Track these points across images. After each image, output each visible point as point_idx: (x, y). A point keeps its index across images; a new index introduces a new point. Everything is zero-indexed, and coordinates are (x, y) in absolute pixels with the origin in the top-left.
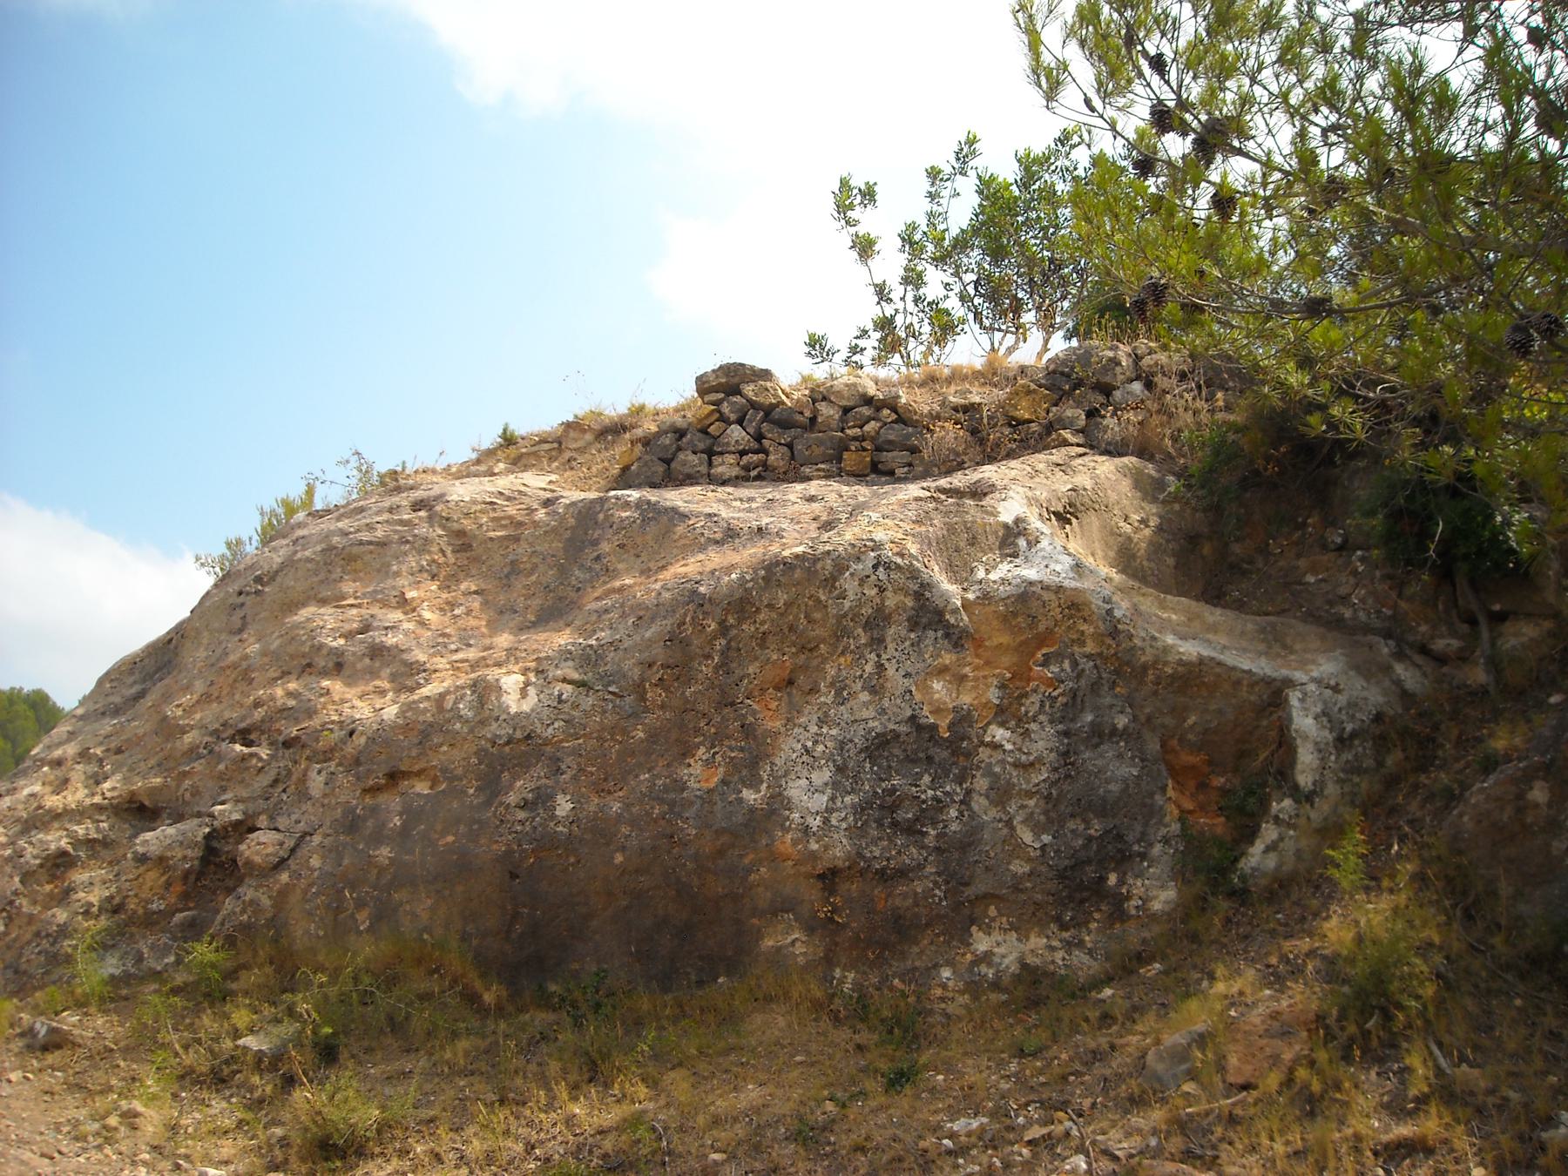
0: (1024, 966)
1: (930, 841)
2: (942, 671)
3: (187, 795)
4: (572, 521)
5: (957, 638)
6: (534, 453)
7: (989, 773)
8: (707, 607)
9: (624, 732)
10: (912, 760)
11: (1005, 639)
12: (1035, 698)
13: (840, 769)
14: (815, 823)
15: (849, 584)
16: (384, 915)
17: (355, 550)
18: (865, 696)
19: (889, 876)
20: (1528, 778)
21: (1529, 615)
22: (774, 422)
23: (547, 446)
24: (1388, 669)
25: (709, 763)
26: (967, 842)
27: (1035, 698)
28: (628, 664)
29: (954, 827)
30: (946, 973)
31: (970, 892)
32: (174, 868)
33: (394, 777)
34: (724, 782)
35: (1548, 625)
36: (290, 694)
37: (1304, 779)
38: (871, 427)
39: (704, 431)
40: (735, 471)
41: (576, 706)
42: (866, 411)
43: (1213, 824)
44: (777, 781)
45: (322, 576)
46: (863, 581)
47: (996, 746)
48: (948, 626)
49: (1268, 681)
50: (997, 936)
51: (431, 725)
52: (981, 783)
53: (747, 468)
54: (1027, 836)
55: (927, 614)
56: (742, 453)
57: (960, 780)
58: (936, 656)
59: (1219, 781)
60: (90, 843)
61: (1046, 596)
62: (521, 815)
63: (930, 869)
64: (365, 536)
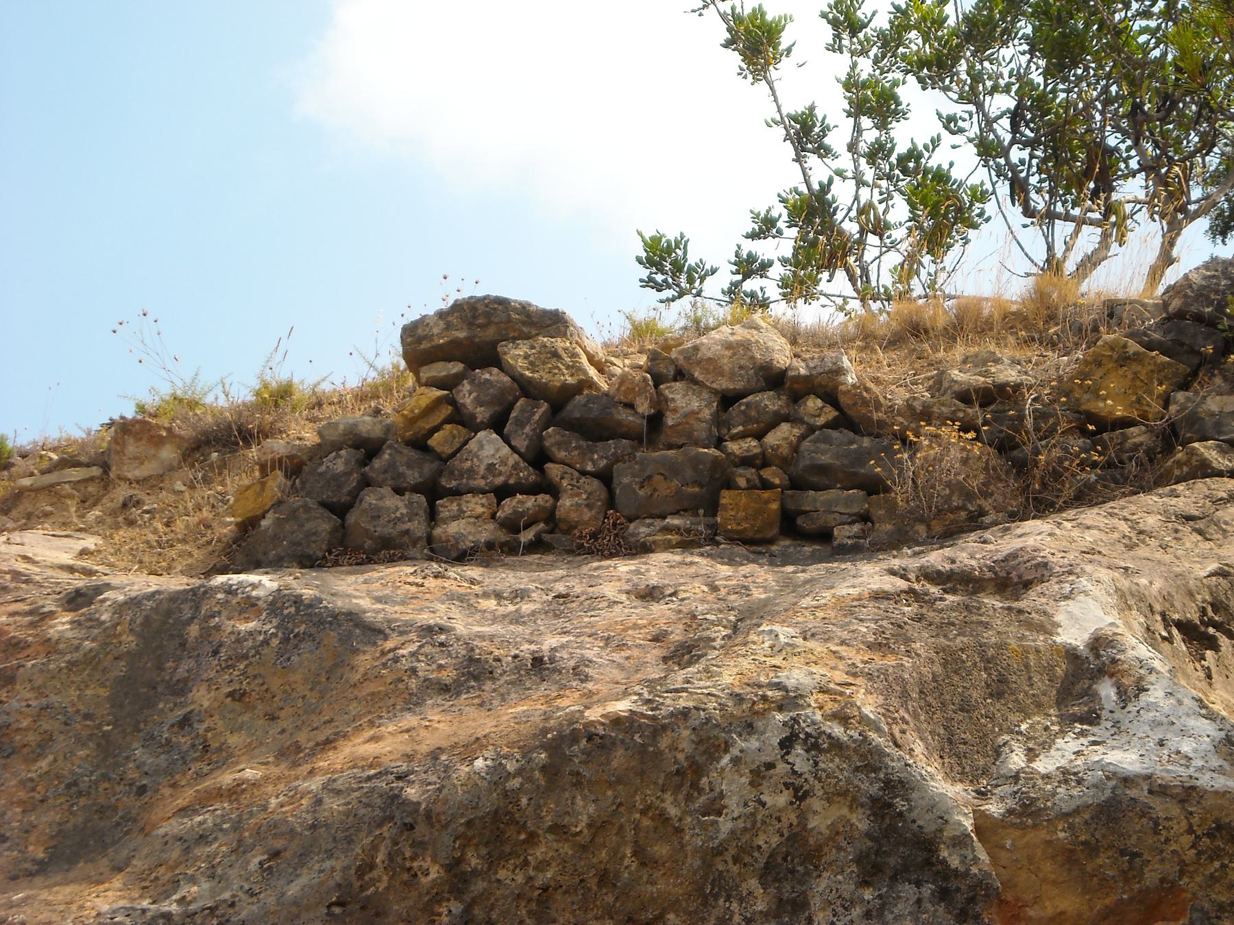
6: (49, 489)
8: (421, 830)
15: (730, 784)
23: (76, 474)
39: (420, 444)
40: (487, 532)
42: (770, 402)
46: (759, 774)
48: (946, 873)
56: (503, 492)
61: (1161, 807)
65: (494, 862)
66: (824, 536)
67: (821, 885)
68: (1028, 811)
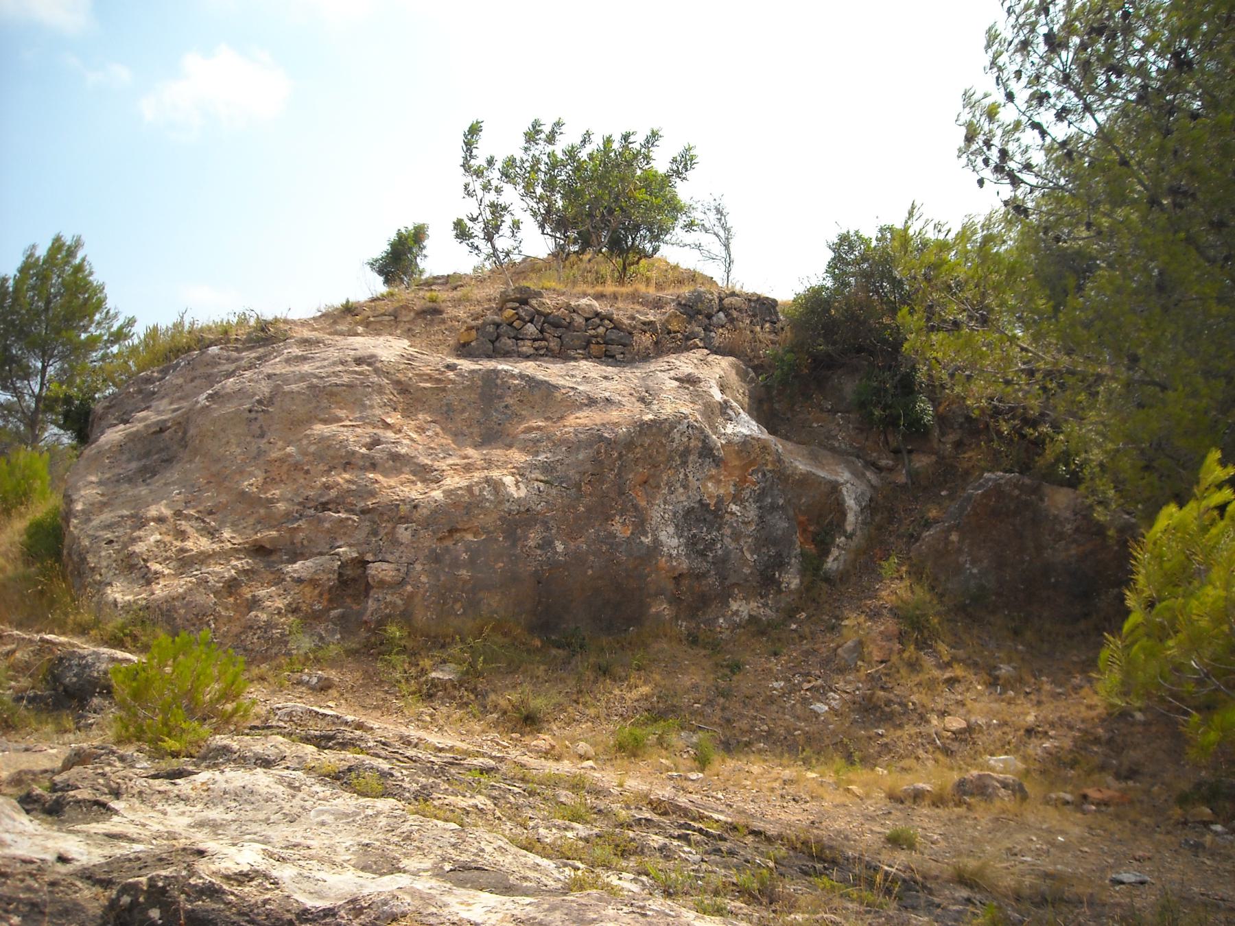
0: (750, 616)
1: (710, 559)
2: (711, 477)
3: (305, 542)
4: (480, 383)
5: (718, 462)
6: (380, 322)
7: (731, 526)
8: (613, 445)
9: (574, 507)
10: (698, 520)
11: (737, 463)
12: (748, 491)
13: (677, 526)
14: (674, 553)
15: (675, 434)
16: (473, 605)
17: (335, 389)
18: (681, 490)
19: (700, 576)
20: (949, 530)
21: (924, 452)
22: (549, 323)
23: (387, 318)
24: (864, 474)
25: (624, 524)
26: (724, 560)
27: (748, 491)
28: (571, 473)
29: (720, 552)
30: (721, 621)
31: (727, 583)
32: (323, 585)
33: (452, 531)
34: (632, 534)
35: (934, 458)
36: (348, 481)
37: (849, 528)
38: (601, 330)
39: (510, 325)
40: (532, 351)
41: (548, 494)
42: (597, 320)
43: (811, 548)
44: (655, 531)
45: (314, 404)
46: (682, 434)
47: (733, 514)
48: (714, 456)
49: (830, 482)
50: (739, 603)
51: (470, 504)
52: (727, 531)
53: (536, 349)
54: (749, 557)
55: (707, 451)
56: (535, 340)
57: (719, 529)
58: (709, 470)
59: (811, 528)
60: (245, 572)
61: (754, 442)
62: (539, 552)
63: (713, 573)
64: (334, 380)
65: (628, 452)
66: (613, 357)
67: (691, 458)
68: (729, 442)
